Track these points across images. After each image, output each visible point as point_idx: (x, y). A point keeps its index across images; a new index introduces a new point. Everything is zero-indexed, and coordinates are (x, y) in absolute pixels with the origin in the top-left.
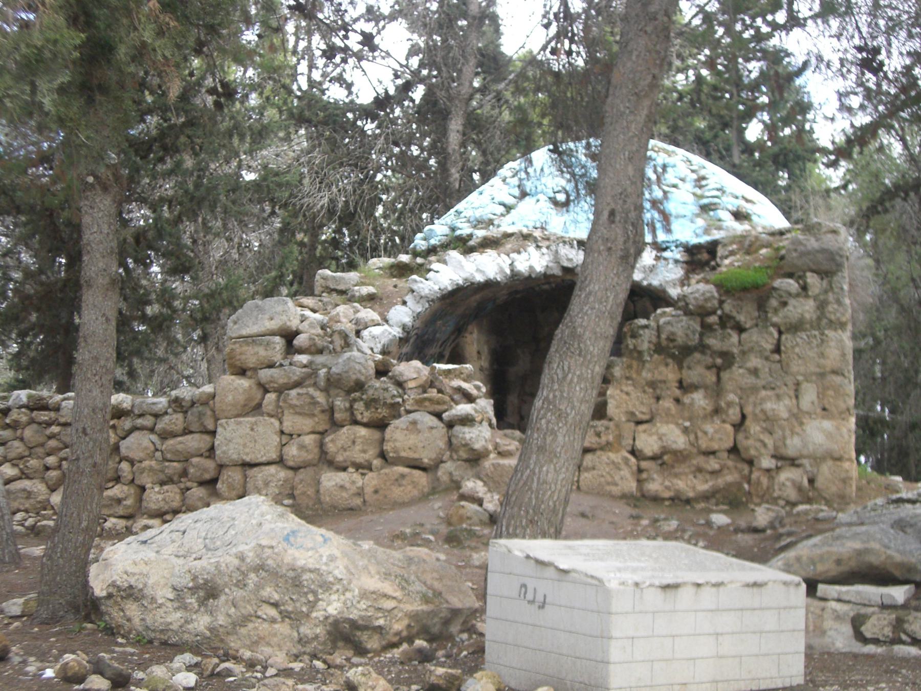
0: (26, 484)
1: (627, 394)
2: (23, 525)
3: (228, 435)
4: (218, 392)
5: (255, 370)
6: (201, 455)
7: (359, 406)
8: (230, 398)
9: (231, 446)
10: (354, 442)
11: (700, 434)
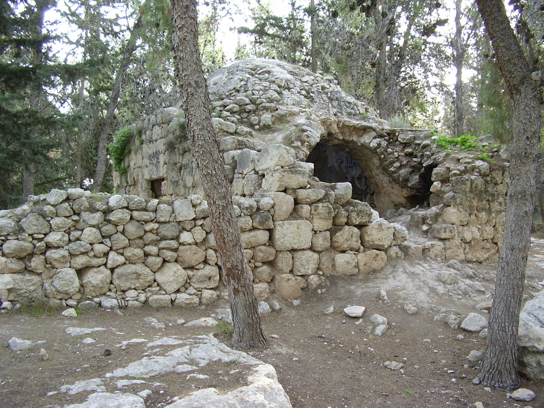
0: (130, 268)
1: (460, 212)
2: (137, 300)
3: (284, 232)
4: (277, 204)
5: (294, 190)
6: (265, 245)
7: (354, 215)
8: (285, 208)
9: (286, 238)
10: (352, 236)
11: (484, 231)
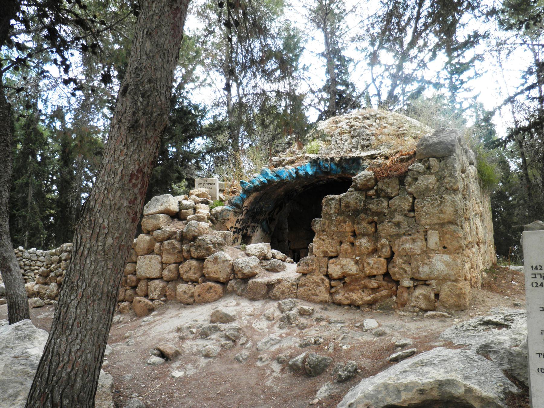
1: (323, 240)
9: (142, 269)
